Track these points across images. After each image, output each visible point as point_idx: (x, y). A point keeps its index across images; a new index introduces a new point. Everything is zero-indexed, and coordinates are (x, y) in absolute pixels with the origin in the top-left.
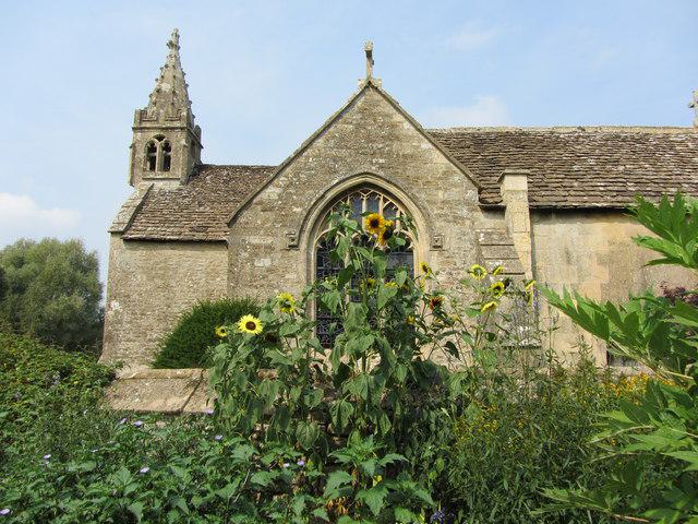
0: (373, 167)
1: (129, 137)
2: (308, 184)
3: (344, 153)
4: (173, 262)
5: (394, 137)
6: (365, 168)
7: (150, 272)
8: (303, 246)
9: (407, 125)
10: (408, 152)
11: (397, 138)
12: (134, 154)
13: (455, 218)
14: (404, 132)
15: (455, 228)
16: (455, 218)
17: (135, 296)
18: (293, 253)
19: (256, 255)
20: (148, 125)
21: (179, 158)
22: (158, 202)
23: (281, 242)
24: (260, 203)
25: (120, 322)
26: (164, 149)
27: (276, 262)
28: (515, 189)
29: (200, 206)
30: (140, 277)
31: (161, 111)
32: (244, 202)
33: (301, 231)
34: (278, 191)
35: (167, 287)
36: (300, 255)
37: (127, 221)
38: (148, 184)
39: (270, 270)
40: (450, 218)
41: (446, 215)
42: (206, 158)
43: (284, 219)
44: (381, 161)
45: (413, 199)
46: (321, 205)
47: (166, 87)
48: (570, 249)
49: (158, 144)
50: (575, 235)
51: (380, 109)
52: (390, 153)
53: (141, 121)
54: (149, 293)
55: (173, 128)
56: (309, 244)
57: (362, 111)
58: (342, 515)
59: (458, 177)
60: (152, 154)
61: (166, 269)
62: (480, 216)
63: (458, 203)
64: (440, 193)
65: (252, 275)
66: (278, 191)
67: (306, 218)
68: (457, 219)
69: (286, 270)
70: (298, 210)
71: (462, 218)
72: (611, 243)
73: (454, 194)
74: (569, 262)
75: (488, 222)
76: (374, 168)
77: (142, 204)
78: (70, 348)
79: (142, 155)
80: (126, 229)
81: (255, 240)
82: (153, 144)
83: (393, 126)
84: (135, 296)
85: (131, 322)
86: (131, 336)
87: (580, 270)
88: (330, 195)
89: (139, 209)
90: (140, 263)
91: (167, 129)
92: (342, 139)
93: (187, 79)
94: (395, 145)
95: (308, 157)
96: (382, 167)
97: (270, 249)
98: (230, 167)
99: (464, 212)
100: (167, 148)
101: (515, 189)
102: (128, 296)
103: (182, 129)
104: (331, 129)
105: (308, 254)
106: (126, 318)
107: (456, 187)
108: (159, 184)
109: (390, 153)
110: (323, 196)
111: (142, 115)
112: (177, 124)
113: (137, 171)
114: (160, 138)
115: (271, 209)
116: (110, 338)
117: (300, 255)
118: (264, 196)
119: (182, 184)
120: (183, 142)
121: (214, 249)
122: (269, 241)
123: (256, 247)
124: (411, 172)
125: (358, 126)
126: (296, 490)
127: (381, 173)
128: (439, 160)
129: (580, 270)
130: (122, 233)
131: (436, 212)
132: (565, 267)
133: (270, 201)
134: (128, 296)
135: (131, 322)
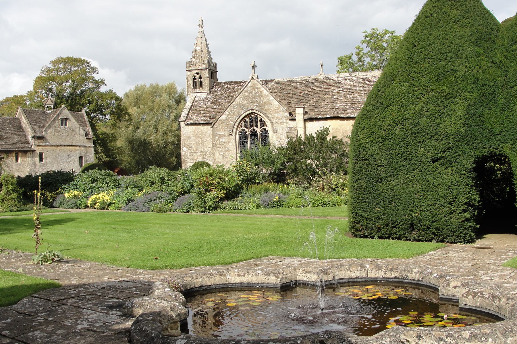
0: (254, 108)
3: (245, 102)
4: (204, 132)
5: (261, 96)
7: (196, 136)
8: (234, 134)
10: (266, 101)
11: (262, 96)
12: (187, 82)
13: (281, 123)
14: (264, 94)
15: (281, 126)
16: (281, 123)
18: (231, 136)
21: (206, 82)
22: (198, 104)
23: (227, 133)
24: (220, 121)
25: (187, 156)
27: (226, 140)
28: (299, 112)
29: (214, 105)
30: (193, 138)
31: (197, 61)
34: (226, 116)
35: (202, 141)
36: (233, 137)
37: (186, 115)
38: (194, 95)
39: (224, 142)
40: (280, 123)
42: (221, 77)
44: (257, 104)
45: (267, 117)
47: (198, 49)
49: (197, 77)
51: (256, 86)
52: (260, 102)
54: (196, 144)
57: (251, 87)
58: (471, 295)
59: (282, 109)
60: (195, 81)
61: (201, 134)
62: (289, 121)
63: (282, 117)
64: (276, 114)
65: (219, 144)
69: (229, 143)
70: (232, 122)
71: (283, 123)
73: (281, 114)
75: (292, 123)
76: (255, 107)
79: (191, 82)
80: (186, 120)
81: (219, 133)
82: (195, 77)
83: (261, 92)
84: (191, 146)
88: (241, 117)
91: (200, 69)
92: (244, 97)
94: (262, 99)
95: (234, 105)
96: (257, 107)
97: (224, 135)
98: (229, 82)
99: (284, 120)
100: (201, 78)
101: (299, 112)
102: (189, 146)
103: (206, 69)
104: (241, 94)
106: (189, 154)
107: (281, 112)
108: (198, 95)
109: (260, 102)
112: (204, 67)
114: (198, 74)
115: (224, 123)
116: (184, 162)
117: (233, 137)
118: (221, 118)
119: (208, 94)
120: (207, 75)
121: (41, 282)
122: (224, 133)
123: (220, 135)
124: (267, 108)
125: (250, 93)
126: (319, 236)
127: (257, 109)
130: (185, 121)
131: (275, 121)
134: (189, 146)
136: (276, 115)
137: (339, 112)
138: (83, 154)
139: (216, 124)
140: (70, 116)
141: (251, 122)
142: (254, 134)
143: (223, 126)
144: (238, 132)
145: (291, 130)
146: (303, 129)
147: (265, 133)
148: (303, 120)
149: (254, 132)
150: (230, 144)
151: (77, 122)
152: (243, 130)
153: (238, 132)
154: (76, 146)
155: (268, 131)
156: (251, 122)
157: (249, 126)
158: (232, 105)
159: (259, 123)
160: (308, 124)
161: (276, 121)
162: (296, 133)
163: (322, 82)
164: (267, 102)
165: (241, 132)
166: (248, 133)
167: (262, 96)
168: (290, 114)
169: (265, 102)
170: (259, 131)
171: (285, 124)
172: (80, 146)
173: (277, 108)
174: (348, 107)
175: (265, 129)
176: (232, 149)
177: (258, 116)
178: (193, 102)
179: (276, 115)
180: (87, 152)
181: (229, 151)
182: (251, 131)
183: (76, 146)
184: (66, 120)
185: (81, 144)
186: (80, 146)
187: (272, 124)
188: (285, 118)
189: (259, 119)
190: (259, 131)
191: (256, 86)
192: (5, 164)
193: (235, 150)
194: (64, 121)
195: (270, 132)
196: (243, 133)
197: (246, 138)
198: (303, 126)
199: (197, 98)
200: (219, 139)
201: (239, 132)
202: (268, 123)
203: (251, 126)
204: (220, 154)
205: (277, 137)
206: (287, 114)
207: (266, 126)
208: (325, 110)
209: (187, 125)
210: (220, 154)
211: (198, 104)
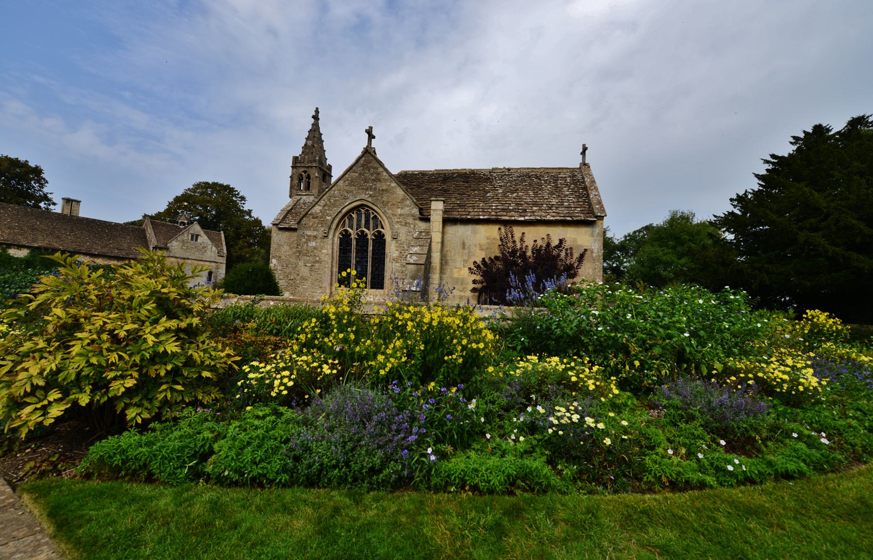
1: (289, 171)
2: (334, 205)
6: (363, 196)
8: (331, 236)
9: (385, 173)
17: (283, 257)
18: (326, 240)
19: (309, 240)
20: (299, 165)
23: (320, 234)
24: (312, 214)
26: (307, 178)
27: (318, 244)
28: (437, 207)
30: (286, 248)
32: (304, 213)
33: (330, 229)
34: (320, 208)
39: (315, 248)
40: (403, 224)
41: (401, 222)
43: (323, 223)
46: (340, 216)
48: (466, 241)
50: (469, 233)
51: (372, 165)
53: (296, 163)
55: (311, 167)
56: (334, 236)
57: (363, 165)
63: (408, 215)
65: (307, 250)
66: (320, 208)
67: (332, 222)
68: (406, 224)
71: (409, 224)
72: (488, 239)
73: (406, 210)
74: (464, 248)
75: (422, 225)
77: (292, 209)
78: (793, 406)
80: (280, 222)
81: (309, 233)
82: (301, 175)
83: (378, 174)
85: (281, 270)
86: (281, 277)
87: (469, 252)
88: (344, 211)
89: (289, 212)
90: (287, 241)
91: (308, 167)
93: (323, 137)
94: (378, 185)
96: (370, 196)
97: (315, 237)
99: (410, 220)
100: (309, 177)
101: (437, 207)
103: (316, 167)
104: (347, 176)
105: (333, 240)
108: (305, 197)
110: (340, 211)
111: (295, 159)
112: (314, 165)
113: (293, 190)
114: (305, 172)
115: (317, 218)
117: (329, 240)
118: (313, 211)
122: (315, 233)
123: (310, 236)
127: (370, 199)
128: (400, 192)
129: (469, 252)
132: (461, 251)
133: (317, 213)
135: (281, 270)
136: (399, 211)
137: (499, 214)
138: (213, 270)
139: (304, 219)
140: (202, 233)
141: (359, 221)
142: (362, 237)
143: (315, 223)
144: (337, 234)
145: (420, 235)
146: (440, 235)
147: (380, 240)
148: (441, 220)
149: (362, 237)
150: (323, 251)
151: (209, 238)
152: (346, 231)
153: (337, 234)
154: (206, 261)
155: (384, 235)
156: (359, 221)
157: (355, 226)
158: (332, 192)
159: (371, 222)
160: (452, 230)
161: (399, 220)
162: (429, 240)
163: (468, 177)
164: (386, 190)
165: (343, 235)
166: (352, 236)
167: (379, 180)
168: (421, 210)
169: (383, 190)
170: (370, 234)
171: (412, 226)
172: (210, 262)
173: (402, 199)
174: (511, 208)
175: (379, 232)
176: (326, 259)
177: (371, 211)
178: (295, 205)
179: (399, 211)
180: (217, 268)
181: (320, 263)
182: (357, 234)
183: (206, 261)
184: (197, 236)
185: (212, 260)
186: (210, 262)
187: (391, 224)
188: (413, 216)
189: (372, 216)
190: (370, 234)
191: (372, 165)
192: (718, 361)
193: (330, 261)
194: (195, 237)
195: (388, 238)
196: (345, 240)
197: (349, 243)
198: (441, 230)
199: (302, 201)
200: (306, 242)
201: (341, 233)
202: (386, 224)
203: (359, 226)
204: (306, 266)
205: (397, 245)
206: (416, 211)
207: (382, 228)
208: (475, 210)
209: (280, 229)
210: (306, 266)
211: (301, 208)
